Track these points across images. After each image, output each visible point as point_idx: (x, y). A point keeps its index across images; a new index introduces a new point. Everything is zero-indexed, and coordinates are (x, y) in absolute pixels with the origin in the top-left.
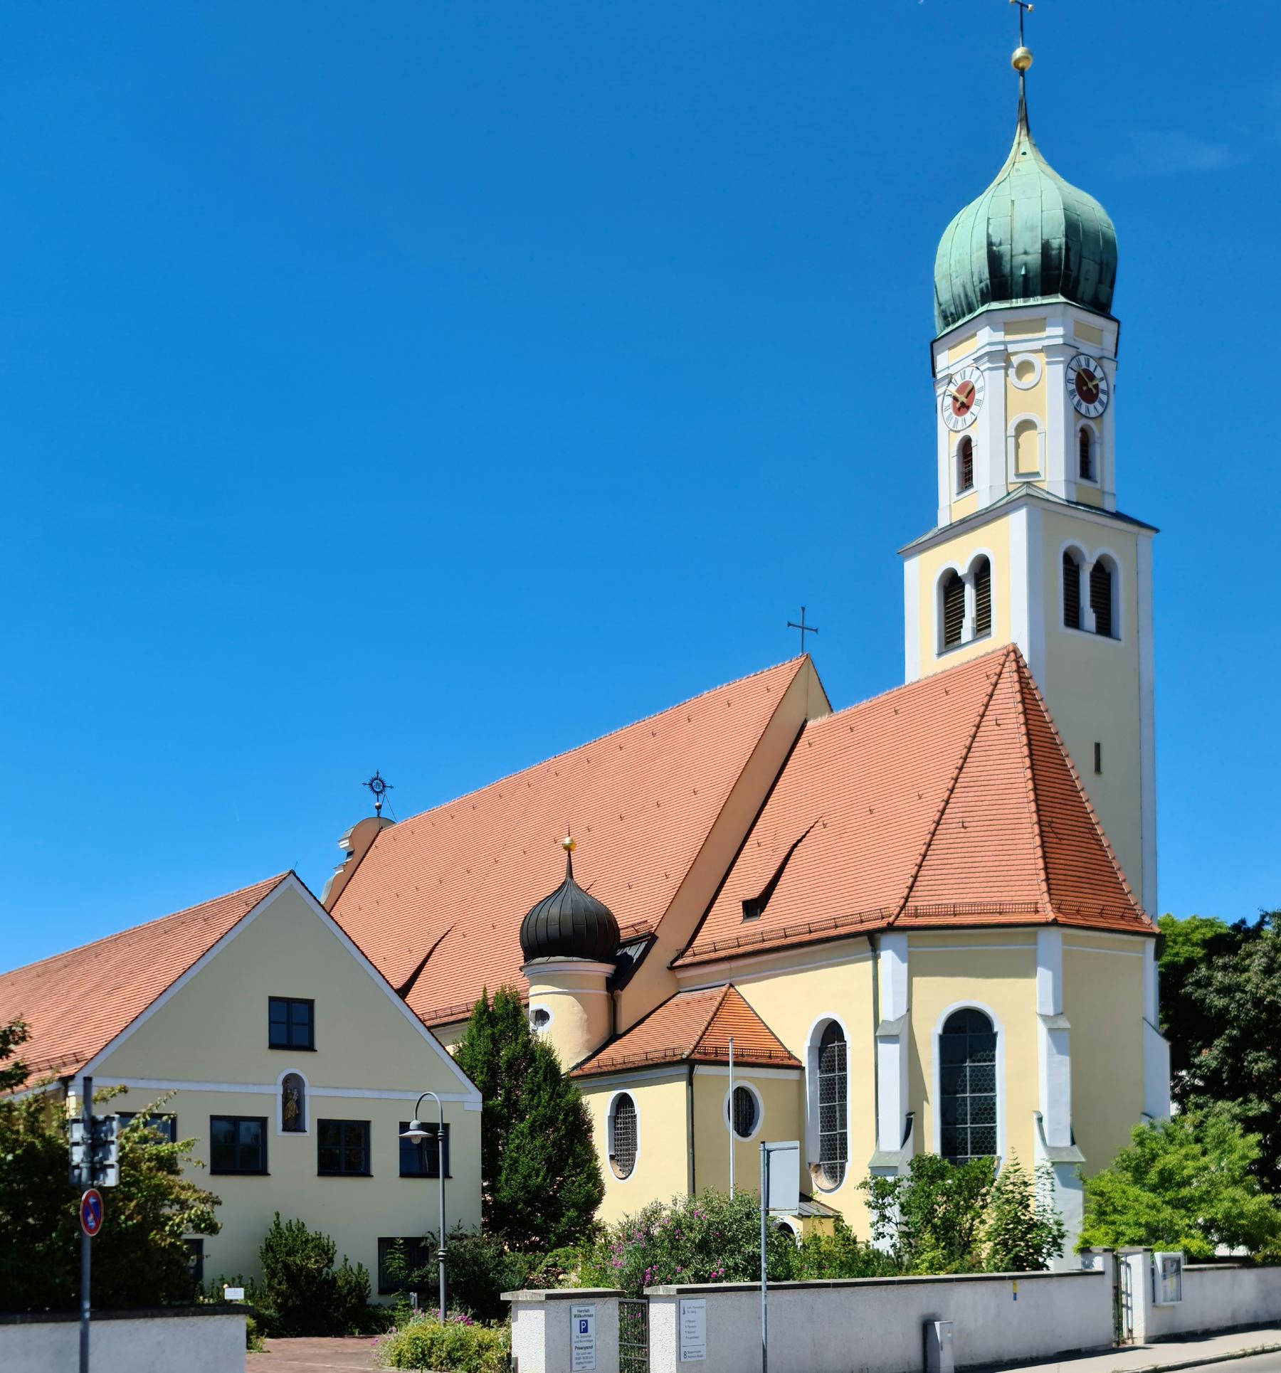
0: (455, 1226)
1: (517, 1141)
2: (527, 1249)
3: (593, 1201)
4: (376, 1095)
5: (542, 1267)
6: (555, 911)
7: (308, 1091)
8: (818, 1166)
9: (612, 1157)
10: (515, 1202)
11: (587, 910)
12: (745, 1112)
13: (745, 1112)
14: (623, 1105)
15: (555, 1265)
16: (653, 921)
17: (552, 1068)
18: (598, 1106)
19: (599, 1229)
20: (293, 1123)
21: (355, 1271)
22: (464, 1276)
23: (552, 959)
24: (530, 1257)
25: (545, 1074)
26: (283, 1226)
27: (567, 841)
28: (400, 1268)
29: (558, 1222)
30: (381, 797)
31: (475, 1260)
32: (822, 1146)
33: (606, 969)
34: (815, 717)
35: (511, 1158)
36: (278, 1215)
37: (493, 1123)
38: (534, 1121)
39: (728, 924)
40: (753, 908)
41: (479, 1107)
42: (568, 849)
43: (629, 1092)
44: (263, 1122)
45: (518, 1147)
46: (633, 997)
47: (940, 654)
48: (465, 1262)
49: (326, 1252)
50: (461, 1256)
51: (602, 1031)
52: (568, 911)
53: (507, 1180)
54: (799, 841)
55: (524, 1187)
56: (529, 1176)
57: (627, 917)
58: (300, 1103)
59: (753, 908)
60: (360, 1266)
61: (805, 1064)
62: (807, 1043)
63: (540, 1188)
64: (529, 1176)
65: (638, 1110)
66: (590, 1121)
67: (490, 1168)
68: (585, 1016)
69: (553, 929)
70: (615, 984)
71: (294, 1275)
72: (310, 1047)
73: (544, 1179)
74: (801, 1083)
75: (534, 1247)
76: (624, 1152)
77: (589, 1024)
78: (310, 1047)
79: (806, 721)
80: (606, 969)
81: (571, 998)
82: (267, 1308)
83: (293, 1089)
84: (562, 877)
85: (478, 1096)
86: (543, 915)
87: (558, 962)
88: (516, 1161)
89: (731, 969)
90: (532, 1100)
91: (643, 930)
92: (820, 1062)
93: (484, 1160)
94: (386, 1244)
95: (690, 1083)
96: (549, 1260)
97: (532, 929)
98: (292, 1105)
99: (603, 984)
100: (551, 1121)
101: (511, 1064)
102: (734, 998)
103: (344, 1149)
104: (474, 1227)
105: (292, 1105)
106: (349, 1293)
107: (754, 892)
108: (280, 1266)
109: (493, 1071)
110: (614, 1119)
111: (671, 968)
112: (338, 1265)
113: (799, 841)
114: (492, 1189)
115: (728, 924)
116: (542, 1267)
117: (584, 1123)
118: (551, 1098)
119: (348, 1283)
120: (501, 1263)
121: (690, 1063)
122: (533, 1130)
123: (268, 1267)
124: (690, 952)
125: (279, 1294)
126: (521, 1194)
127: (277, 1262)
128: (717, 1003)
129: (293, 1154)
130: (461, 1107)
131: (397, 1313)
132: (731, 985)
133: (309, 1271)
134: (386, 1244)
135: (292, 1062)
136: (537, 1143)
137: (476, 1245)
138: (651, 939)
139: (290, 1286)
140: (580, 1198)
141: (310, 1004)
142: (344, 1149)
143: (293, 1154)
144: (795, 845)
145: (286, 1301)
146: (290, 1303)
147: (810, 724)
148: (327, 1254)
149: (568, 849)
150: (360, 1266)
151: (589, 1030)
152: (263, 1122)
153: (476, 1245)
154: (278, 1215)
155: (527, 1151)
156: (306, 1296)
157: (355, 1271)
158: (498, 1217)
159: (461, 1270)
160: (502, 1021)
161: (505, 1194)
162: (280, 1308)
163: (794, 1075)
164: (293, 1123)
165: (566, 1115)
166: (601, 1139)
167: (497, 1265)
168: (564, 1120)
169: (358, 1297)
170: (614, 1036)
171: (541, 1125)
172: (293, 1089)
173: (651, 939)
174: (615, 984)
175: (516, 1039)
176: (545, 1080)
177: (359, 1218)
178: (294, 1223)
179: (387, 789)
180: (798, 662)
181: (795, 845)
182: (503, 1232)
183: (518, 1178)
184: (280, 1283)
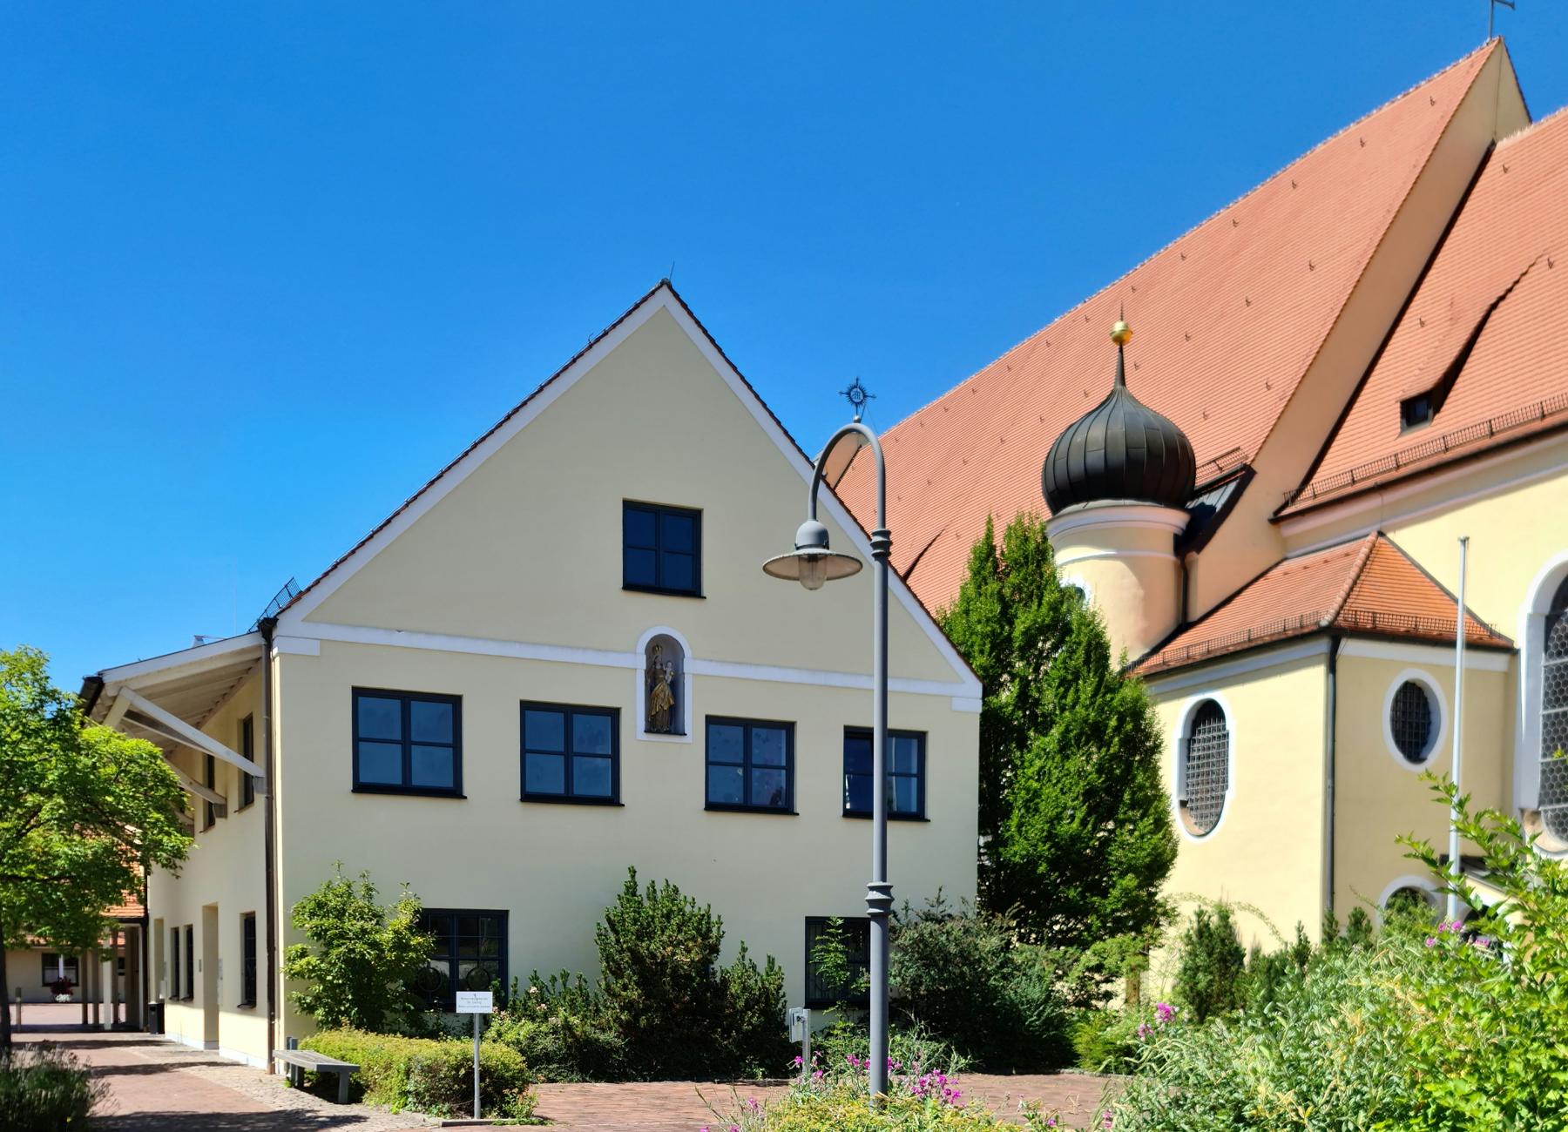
0: (933, 899)
1: (1038, 763)
2: (1055, 941)
3: (1158, 866)
4: (804, 677)
5: (1077, 971)
6: (1097, 432)
7: (690, 667)
8: (1536, 813)
9: (1183, 804)
10: (1032, 862)
11: (1149, 428)
12: (1414, 721)
13: (1414, 721)
14: (1208, 714)
15: (1099, 968)
16: (1249, 451)
17: (1097, 651)
18: (1170, 718)
19: (799, 1043)
20: (664, 720)
21: (762, 968)
22: (945, 982)
23: (1092, 504)
24: (1056, 952)
25: (1088, 653)
26: (642, 890)
27: (1119, 327)
28: (838, 966)
29: (1104, 894)
30: (861, 408)
31: (965, 957)
32: (1545, 779)
33: (1173, 520)
34: (1510, 131)
35: (1028, 790)
36: (633, 872)
37: (999, 736)
38: (1067, 731)
39: (1373, 439)
40: (1417, 409)
41: (978, 707)
42: (1120, 340)
43: (1221, 696)
44: (613, 714)
45: (1041, 773)
46: (1216, 564)
47: (1400, 435)
48: (947, 959)
49: (705, 935)
50: (942, 949)
51: (1165, 617)
52: (1118, 429)
53: (1020, 825)
54: (1502, 298)
55: (1050, 837)
56: (1059, 817)
57: (1210, 448)
58: (676, 687)
59: (1417, 409)
60: (771, 961)
61: (1521, 643)
62: (1528, 608)
63: (1075, 838)
64: (1059, 817)
65: (1231, 723)
66: (1157, 736)
67: (992, 811)
68: (1141, 593)
69: (1096, 458)
70: (1189, 542)
71: (649, 973)
72: (693, 590)
73: (1084, 823)
74: (1510, 677)
75: (1063, 940)
76: (1207, 798)
77: (1147, 601)
78: (693, 590)
79: (1493, 144)
80: (1173, 520)
81: (1119, 565)
82: (603, 1030)
83: (663, 666)
84: (1108, 383)
85: (977, 688)
86: (1079, 438)
87: (1102, 510)
88: (1037, 794)
89: (1383, 506)
90: (1064, 696)
91: (1230, 464)
92: (1547, 638)
93: (983, 797)
94: (816, 925)
95: (1332, 669)
96: (1089, 957)
97: (1061, 463)
98: (663, 689)
99: (1169, 543)
100: (1095, 733)
101: (1030, 639)
102: (1387, 551)
103: (750, 770)
104: (964, 901)
105: (663, 689)
106: (748, 1007)
107: (1426, 380)
108: (627, 956)
109: (1000, 645)
110: (1189, 743)
111: (1277, 519)
112: (725, 962)
113: (1502, 298)
114: (992, 849)
115: (1373, 439)
116: (1077, 971)
117: (1148, 737)
118: (1095, 695)
119: (745, 989)
120: (1007, 962)
121: (1335, 634)
122: (1064, 748)
123: (609, 958)
124: (1308, 492)
125: (628, 1006)
126: (1043, 848)
127: (621, 952)
128: (1359, 562)
129: (663, 772)
130: (946, 706)
131: (832, 1041)
132: (1381, 534)
133: (676, 967)
134: (816, 925)
135: (662, 614)
136: (1071, 765)
137: (967, 931)
138: (1245, 475)
139: (647, 995)
140: (1143, 857)
141: (695, 516)
142: (750, 770)
143: (663, 772)
144: (1494, 306)
145: (636, 1018)
146: (643, 1021)
147: (1500, 146)
148: (706, 936)
149: (1120, 340)
150: (771, 961)
151: (1147, 614)
152: (613, 714)
153: (967, 931)
154: (633, 872)
155: (1054, 780)
156: (683, 1015)
157: (762, 968)
158: (1005, 887)
159: (941, 971)
160: (1014, 578)
161: (1017, 851)
162: (628, 1029)
163: (1498, 662)
164: (664, 720)
165: (1121, 721)
166: (1169, 765)
167: (1002, 965)
168: (1117, 729)
169: (763, 1013)
170: (1184, 624)
171: (1078, 738)
172: (663, 666)
173: (1245, 475)
174: (1189, 542)
175: (1040, 598)
176: (1087, 662)
177: (768, 887)
178: (660, 886)
179: (869, 400)
180: (1488, 46)
181: (1494, 306)
182: (1012, 911)
183: (1037, 827)
184: (625, 988)
